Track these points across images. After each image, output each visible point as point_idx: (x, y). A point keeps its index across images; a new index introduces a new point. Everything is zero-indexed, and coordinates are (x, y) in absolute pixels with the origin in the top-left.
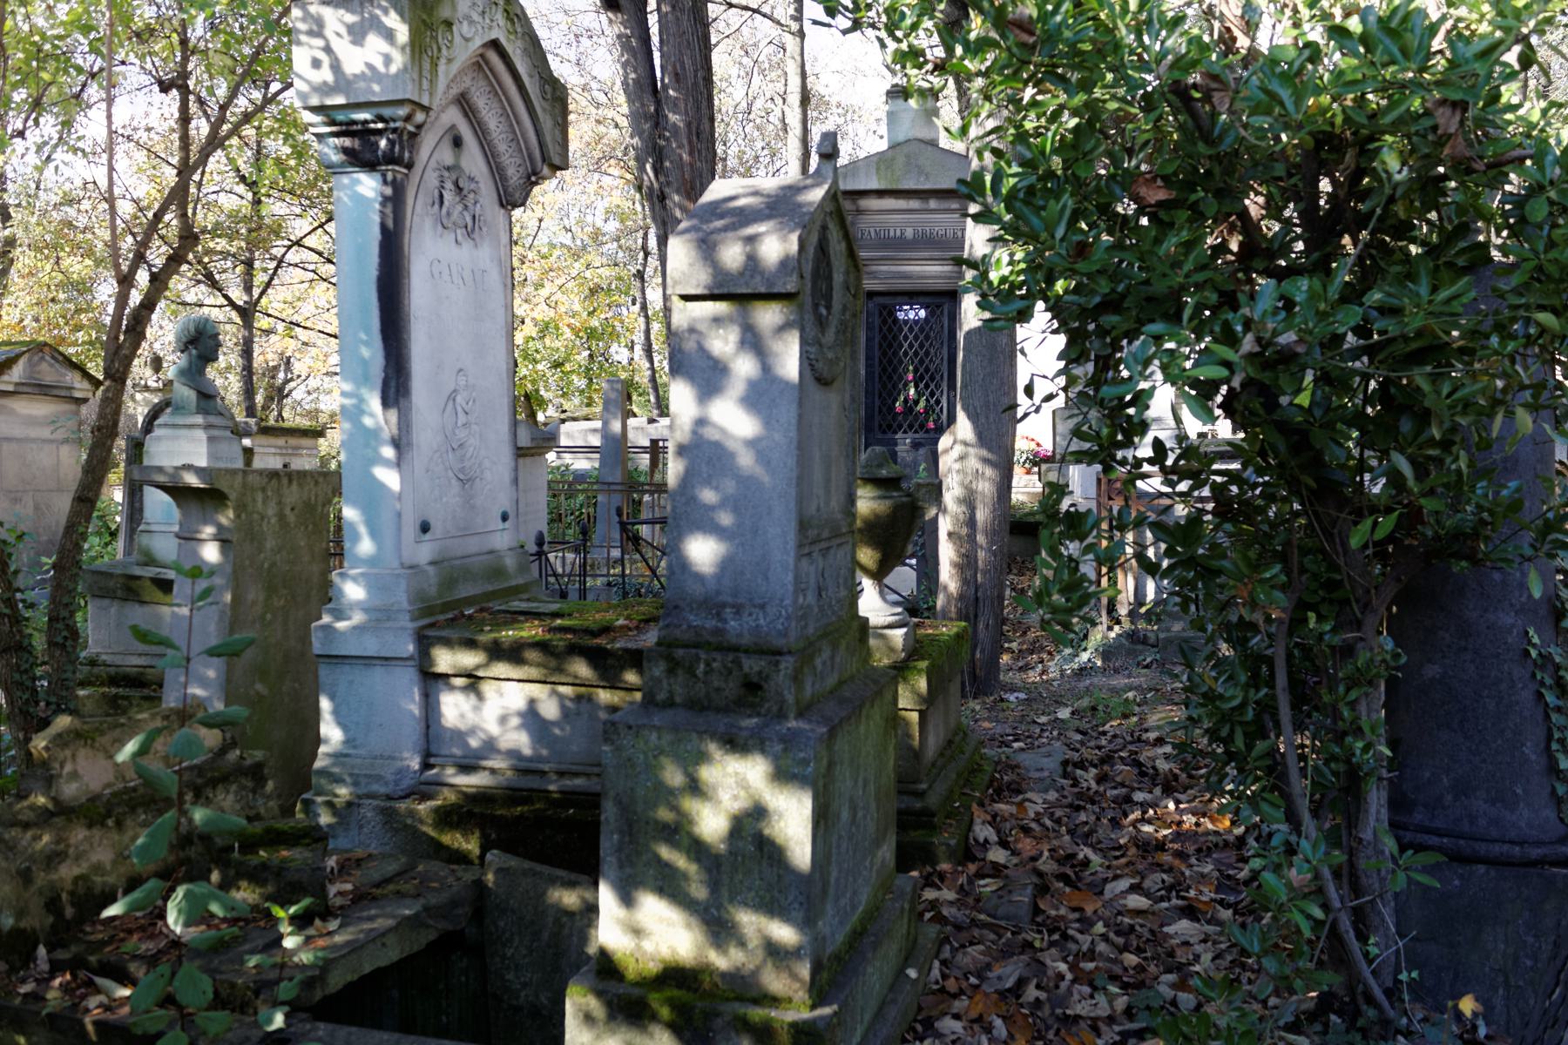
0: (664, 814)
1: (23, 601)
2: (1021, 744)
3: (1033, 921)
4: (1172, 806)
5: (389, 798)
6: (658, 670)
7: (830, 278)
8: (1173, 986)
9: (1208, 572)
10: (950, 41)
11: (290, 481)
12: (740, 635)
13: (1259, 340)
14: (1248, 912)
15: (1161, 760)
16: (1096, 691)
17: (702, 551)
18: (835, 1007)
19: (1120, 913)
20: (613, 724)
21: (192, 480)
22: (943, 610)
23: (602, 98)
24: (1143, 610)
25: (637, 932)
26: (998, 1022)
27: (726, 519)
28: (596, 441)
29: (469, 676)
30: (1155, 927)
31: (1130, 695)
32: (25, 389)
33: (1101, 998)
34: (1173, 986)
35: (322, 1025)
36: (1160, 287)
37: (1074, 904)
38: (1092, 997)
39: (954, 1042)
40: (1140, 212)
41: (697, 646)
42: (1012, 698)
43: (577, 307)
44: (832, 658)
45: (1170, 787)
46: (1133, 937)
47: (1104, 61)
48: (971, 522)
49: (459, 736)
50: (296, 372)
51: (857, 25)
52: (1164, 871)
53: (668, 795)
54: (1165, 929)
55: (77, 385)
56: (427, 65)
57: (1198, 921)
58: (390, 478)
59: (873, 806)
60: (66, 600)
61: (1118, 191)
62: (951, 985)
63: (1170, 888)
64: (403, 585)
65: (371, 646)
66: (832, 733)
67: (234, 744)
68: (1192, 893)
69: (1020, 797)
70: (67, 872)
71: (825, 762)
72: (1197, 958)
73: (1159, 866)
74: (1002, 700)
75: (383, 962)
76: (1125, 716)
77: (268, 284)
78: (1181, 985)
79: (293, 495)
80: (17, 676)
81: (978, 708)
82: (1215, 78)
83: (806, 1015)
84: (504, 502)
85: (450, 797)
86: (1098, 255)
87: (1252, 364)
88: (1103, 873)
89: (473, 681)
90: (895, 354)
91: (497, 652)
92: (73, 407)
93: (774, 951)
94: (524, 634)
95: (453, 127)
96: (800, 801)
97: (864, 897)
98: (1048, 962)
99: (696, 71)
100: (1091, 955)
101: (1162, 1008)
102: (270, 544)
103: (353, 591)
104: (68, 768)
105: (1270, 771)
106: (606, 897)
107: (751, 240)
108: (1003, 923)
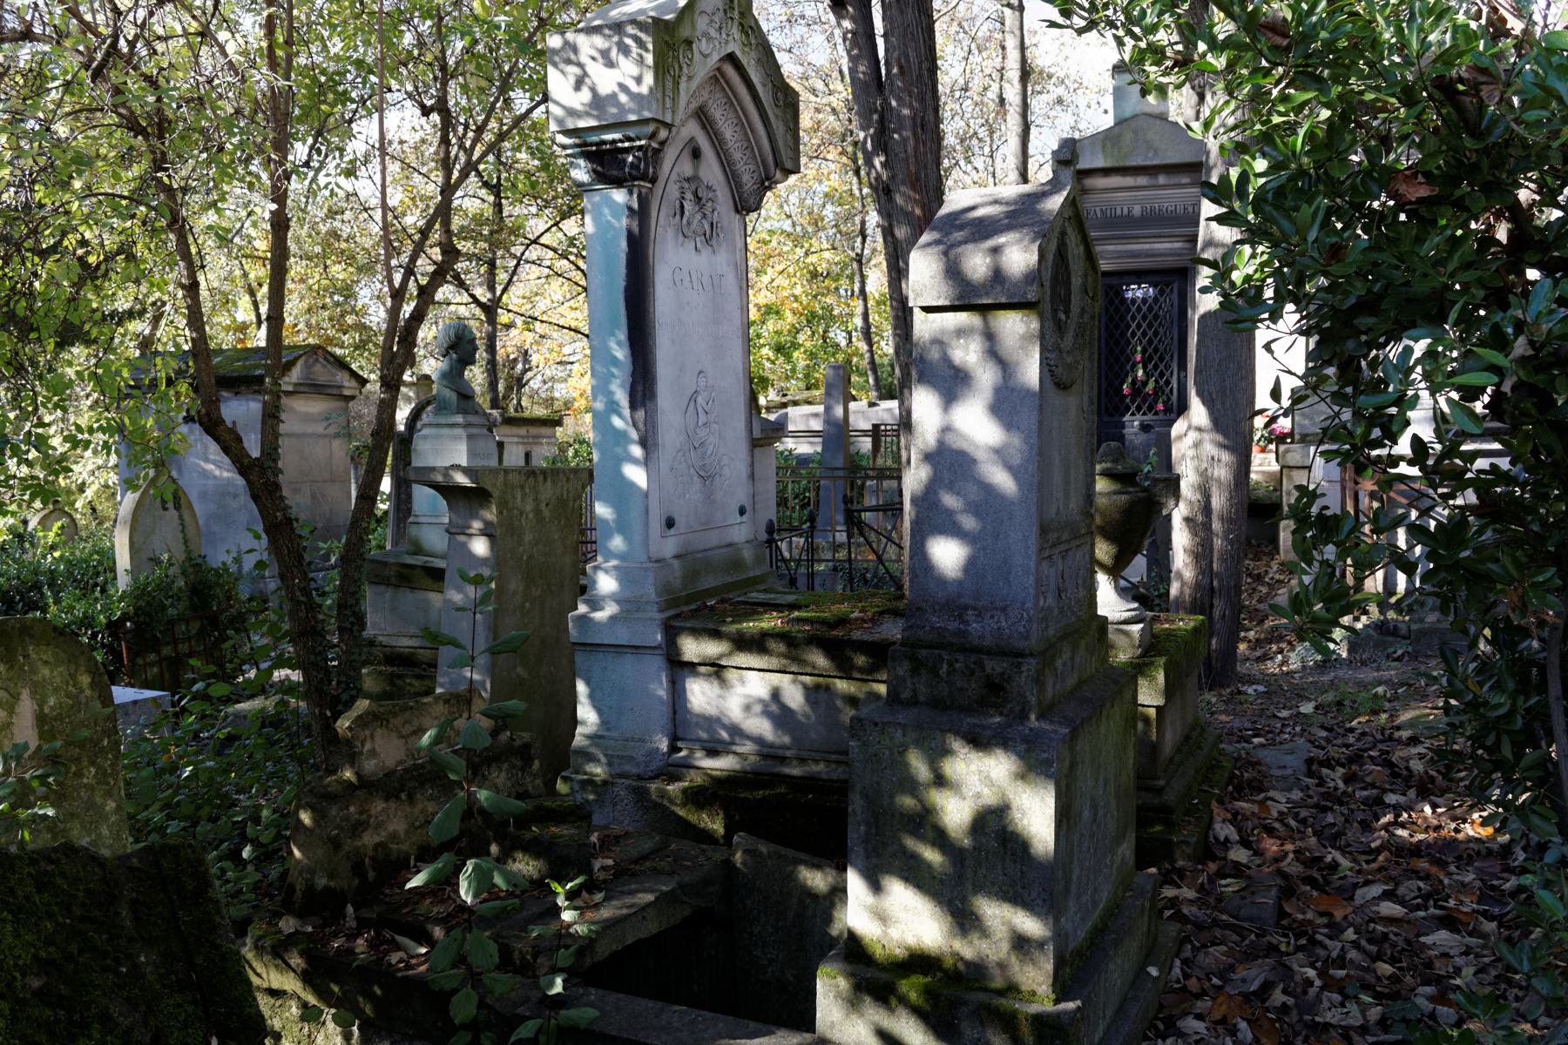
0: (908, 802)
1: (317, 590)
2: (1262, 740)
3: (1278, 924)
4: (1428, 810)
5: (639, 778)
6: (903, 669)
7: (1068, 283)
8: (1431, 999)
9: (1477, 579)
10: (1192, 38)
11: (545, 479)
12: (982, 637)
13: (1532, 343)
14: (1515, 929)
15: (1416, 760)
16: (1342, 685)
17: (947, 554)
18: (1079, 1003)
19: (1372, 920)
20: (860, 720)
21: (461, 479)
22: (1177, 598)
23: (820, 86)
24: (1393, 600)
25: (882, 917)
26: (1243, 1025)
27: (969, 522)
28: (817, 425)
29: (713, 665)
30: (1411, 936)
31: (1380, 690)
32: (302, 389)
33: (1352, 1007)
34: (1431, 999)
35: (593, 991)
36: (1421, 288)
37: (1322, 908)
38: (1343, 1005)
39: (1197, 1042)
40: (1400, 207)
41: (940, 646)
42: (1250, 691)
43: (798, 290)
44: (1072, 659)
45: (1426, 790)
46: (1386, 946)
47: (1363, 57)
48: (1207, 509)
49: (711, 722)
50: (534, 363)
51: (1092, 25)
52: (1421, 879)
53: (911, 785)
54: (1422, 939)
55: (346, 384)
56: (669, 85)
57: (1459, 932)
58: (636, 475)
59: (1113, 804)
60: (352, 589)
61: (1375, 189)
62: (1193, 984)
63: (1426, 897)
64: (651, 579)
65: (622, 636)
66: (1074, 735)
67: (505, 727)
68: (1452, 903)
69: (1262, 796)
70: (369, 839)
71: (1067, 763)
72: (1458, 971)
73: (1416, 874)
74: (1240, 692)
75: (643, 935)
76: (1375, 712)
77: (510, 282)
78: (1440, 999)
79: (548, 491)
80: (312, 657)
81: (1214, 700)
82: (1484, 71)
83: (1049, 1007)
84: (741, 496)
85: (699, 780)
86: (1353, 256)
87: (1524, 368)
88: (1353, 878)
89: (717, 670)
90: (1123, 334)
91: (744, 643)
92: (341, 404)
93: (1021, 943)
94: (764, 625)
95: (692, 139)
96: (1043, 800)
97: (1104, 897)
98: (1296, 967)
99: (920, 63)
100: (1341, 962)
101: (1420, 1021)
102: (528, 537)
103: (606, 583)
104: (368, 746)
105: (1539, 783)
106: (855, 882)
107: (996, 251)
108: (1246, 925)
